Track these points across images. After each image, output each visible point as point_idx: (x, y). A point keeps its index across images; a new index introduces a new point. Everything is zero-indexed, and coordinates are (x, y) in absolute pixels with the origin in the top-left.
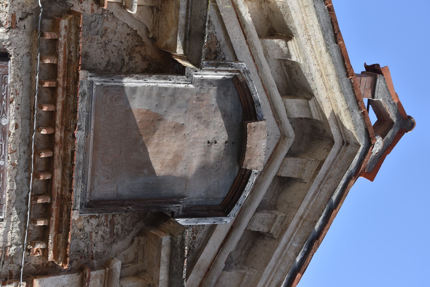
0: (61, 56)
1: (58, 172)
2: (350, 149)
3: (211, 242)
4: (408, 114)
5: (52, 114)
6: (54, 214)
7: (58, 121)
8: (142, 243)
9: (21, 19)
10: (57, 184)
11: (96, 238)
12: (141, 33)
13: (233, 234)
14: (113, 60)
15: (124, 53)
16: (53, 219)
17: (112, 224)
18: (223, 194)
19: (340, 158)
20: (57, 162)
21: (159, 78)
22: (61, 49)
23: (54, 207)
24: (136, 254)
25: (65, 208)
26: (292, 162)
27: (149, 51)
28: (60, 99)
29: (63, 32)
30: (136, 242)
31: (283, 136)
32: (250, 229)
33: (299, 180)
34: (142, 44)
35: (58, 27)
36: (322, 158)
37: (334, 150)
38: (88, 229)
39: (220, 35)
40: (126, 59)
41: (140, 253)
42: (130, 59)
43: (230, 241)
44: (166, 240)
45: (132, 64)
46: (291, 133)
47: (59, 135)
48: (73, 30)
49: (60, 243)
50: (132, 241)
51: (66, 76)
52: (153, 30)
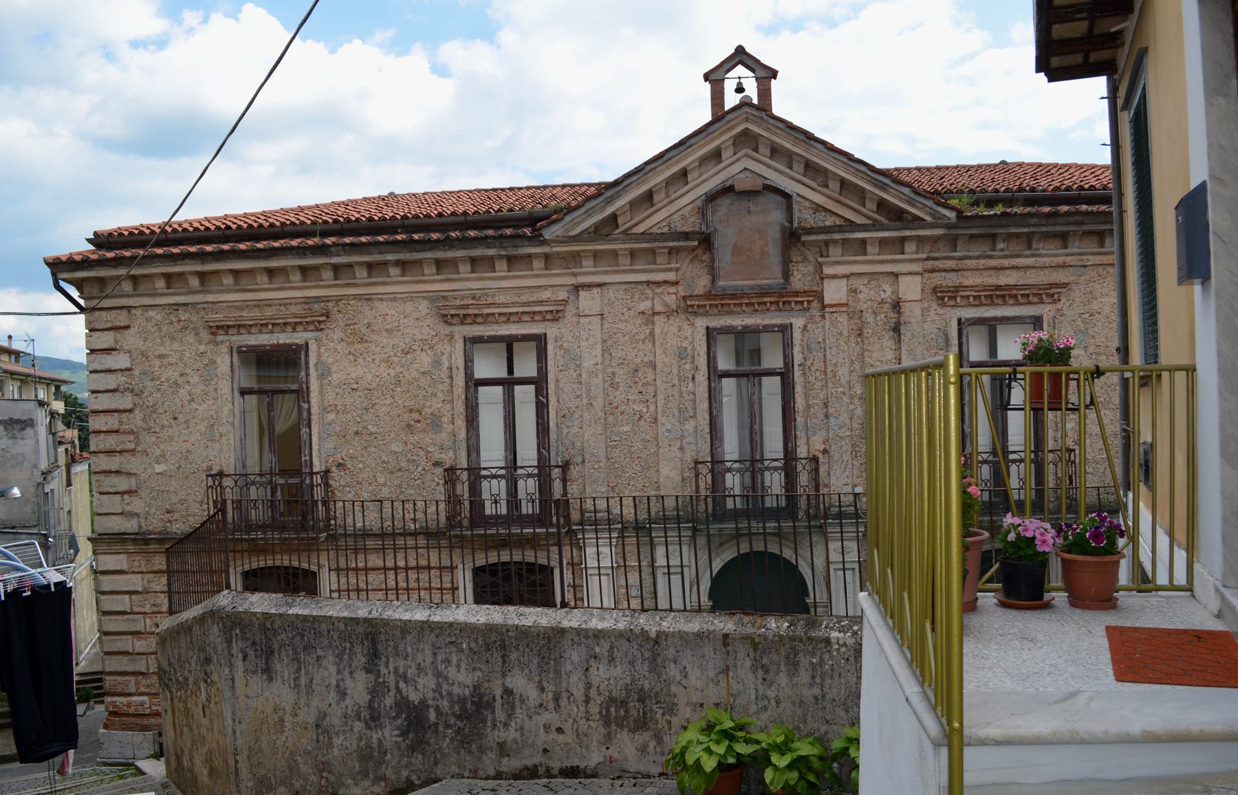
1: (765, 299)
2: (751, 117)
3: (779, 429)
10: (772, 299)
11: (805, 271)
12: (691, 257)
16: (791, 299)
18: (779, 198)
20: (760, 300)
26: (761, 149)
27: (699, 251)
29: (693, 303)
31: (746, 155)
32: (791, 261)
34: (697, 255)
38: (800, 276)
39: (689, 208)
46: (744, 151)
51: (715, 300)
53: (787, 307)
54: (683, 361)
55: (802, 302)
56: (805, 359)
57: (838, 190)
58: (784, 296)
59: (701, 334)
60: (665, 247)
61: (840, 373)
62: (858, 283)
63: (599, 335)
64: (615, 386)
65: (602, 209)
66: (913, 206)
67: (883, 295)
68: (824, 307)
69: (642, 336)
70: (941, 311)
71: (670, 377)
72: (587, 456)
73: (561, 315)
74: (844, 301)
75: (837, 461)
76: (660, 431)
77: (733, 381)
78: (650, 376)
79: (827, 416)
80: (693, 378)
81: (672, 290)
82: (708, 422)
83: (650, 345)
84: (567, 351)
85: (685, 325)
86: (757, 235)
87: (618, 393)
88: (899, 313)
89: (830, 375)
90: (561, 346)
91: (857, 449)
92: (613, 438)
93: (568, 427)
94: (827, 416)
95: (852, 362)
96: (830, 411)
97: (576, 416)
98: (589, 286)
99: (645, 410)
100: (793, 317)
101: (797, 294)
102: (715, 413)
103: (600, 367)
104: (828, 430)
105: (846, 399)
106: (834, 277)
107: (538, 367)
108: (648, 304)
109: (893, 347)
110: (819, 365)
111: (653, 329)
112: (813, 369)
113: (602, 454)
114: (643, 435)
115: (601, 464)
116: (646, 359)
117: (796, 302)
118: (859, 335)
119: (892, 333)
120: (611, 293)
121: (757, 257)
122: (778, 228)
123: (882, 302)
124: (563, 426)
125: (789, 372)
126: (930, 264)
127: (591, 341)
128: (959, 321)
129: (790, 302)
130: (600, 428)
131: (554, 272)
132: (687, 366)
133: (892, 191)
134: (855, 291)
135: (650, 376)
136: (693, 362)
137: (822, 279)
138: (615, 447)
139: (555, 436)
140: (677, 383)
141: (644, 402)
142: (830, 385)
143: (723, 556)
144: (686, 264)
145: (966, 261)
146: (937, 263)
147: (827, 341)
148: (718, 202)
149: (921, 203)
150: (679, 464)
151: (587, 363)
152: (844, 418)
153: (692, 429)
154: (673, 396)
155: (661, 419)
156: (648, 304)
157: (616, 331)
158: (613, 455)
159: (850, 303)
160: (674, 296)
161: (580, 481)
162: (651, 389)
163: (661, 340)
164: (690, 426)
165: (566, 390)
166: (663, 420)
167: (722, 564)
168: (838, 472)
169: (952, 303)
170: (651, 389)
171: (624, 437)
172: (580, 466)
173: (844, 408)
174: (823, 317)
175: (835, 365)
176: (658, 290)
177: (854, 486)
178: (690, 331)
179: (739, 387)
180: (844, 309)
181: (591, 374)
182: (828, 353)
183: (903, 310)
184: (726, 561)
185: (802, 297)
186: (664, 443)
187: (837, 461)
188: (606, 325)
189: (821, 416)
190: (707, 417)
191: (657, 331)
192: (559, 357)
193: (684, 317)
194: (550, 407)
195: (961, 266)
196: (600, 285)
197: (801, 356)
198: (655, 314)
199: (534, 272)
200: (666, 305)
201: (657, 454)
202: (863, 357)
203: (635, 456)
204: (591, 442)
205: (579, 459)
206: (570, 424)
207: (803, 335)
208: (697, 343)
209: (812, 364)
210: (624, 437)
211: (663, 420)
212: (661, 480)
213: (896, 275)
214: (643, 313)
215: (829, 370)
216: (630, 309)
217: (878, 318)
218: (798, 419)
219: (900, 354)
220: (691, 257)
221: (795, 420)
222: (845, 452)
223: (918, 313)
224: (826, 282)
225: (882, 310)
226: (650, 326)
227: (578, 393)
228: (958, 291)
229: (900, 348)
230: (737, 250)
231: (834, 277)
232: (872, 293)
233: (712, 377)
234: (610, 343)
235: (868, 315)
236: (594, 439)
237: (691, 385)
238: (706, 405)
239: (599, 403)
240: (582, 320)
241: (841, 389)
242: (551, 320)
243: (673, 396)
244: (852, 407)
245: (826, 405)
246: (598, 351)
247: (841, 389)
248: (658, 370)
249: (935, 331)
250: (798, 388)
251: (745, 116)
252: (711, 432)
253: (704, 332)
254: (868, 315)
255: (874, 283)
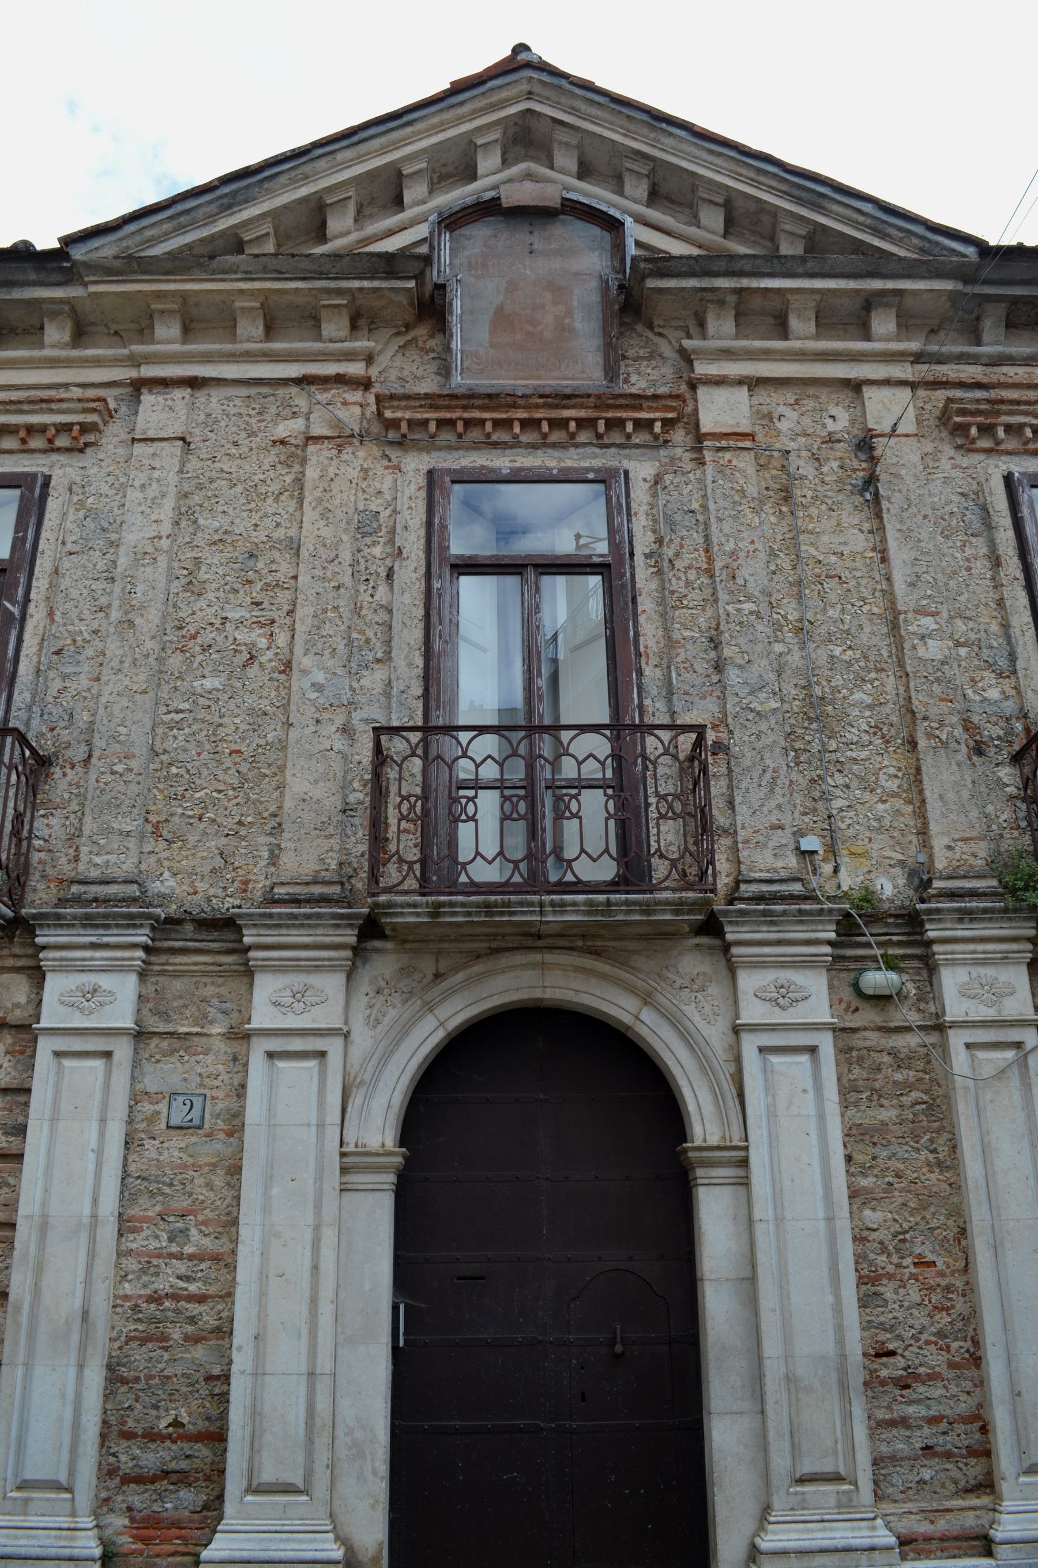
0: (426, 416)
1: (566, 413)
2: (537, 89)
4: (509, 53)
5: (497, 423)
6: (619, 415)
7: (504, 416)
8: (662, 323)
9: (390, 460)
10: (582, 414)
13: (653, 222)
14: (435, 369)
15: (426, 358)
17: (638, 358)
18: (596, 231)
19: (548, 99)
20: (554, 414)
21: (451, 313)
22: (419, 416)
23: (610, 415)
24: (676, 328)
25: (611, 401)
28: (477, 414)
29: (399, 414)
30: (661, 330)
33: (579, 147)
34: (415, 339)
35: (393, 420)
36: (550, 122)
37: (538, 107)
40: (432, 355)
41: (675, 323)
42: (433, 351)
43: (661, 225)
44: (651, 283)
45: (440, 349)
47: (522, 414)
48: (395, 403)
49: (655, 405)
50: (660, 335)
52: (396, 327)
53: (616, 437)
54: (368, 540)
55: (650, 423)
56: (660, 541)
57: (722, 232)
58: (609, 407)
59: (413, 487)
60: (339, 292)
61: (744, 573)
62: (776, 401)
63: (173, 478)
64: (193, 587)
65: (211, 218)
66: (885, 236)
67: (831, 426)
68: (700, 438)
69: (275, 488)
70: (965, 461)
71: (331, 567)
72: (99, 743)
73: (91, 438)
74: (747, 429)
75: (749, 769)
76: (295, 688)
77: (489, 582)
78: (285, 569)
79: (719, 667)
80: (390, 575)
81: (357, 396)
82: (420, 671)
83: (292, 505)
84: (91, 513)
85: (379, 468)
86: (548, 295)
87: (202, 603)
88: (873, 460)
89: (720, 575)
90: (81, 504)
91: (798, 745)
92: (174, 705)
93: (65, 677)
94: (719, 667)
95: (773, 554)
96: (727, 652)
97: (90, 652)
98: (165, 383)
99: (263, 642)
100: (629, 457)
101: (637, 401)
102: (437, 645)
103: (165, 543)
104: (723, 698)
105: (762, 628)
106: (720, 382)
107: (15, 540)
108: (297, 425)
109: (866, 526)
110: (692, 556)
111: (303, 473)
112: (679, 564)
113: (139, 739)
114: (250, 700)
115: (134, 764)
116: (279, 534)
117: (638, 424)
118: (786, 499)
119: (858, 500)
120: (213, 400)
121: (548, 335)
122: (594, 284)
123: (831, 440)
124: (52, 674)
125: (622, 564)
126: (923, 370)
127: (153, 491)
128: (1008, 480)
129: (621, 423)
130: (142, 677)
131: (90, 352)
132: (377, 551)
133: (835, 207)
134: (769, 416)
135: (285, 569)
136: (391, 542)
137: (693, 386)
138: (178, 725)
139: (27, 696)
140: (347, 579)
141: (262, 625)
142: (723, 596)
143: (444, 1011)
144: (389, 354)
145: (1005, 369)
146: (943, 369)
147: (712, 506)
148: (466, 231)
149: (900, 229)
150: (337, 767)
151: (133, 536)
152: (762, 668)
153: (379, 688)
154: (336, 608)
155: (303, 661)
156: (297, 425)
157: (214, 474)
158: (170, 744)
159: (760, 437)
160: (357, 410)
161: (74, 806)
162: (283, 597)
163: (318, 493)
164: (374, 679)
165: (74, 593)
166: (307, 662)
167: (441, 1034)
168: (755, 797)
169: (985, 443)
170: (283, 597)
171: (202, 701)
172: (79, 769)
173: (759, 648)
174: (701, 462)
175: (733, 554)
176: (323, 397)
177: (800, 833)
178: (389, 480)
179: (501, 594)
180: (748, 444)
181: (139, 557)
182: (714, 528)
183: (878, 453)
184: (453, 1024)
185: (650, 409)
186: (302, 714)
187: (749, 769)
188: (193, 464)
189: (701, 667)
190: (420, 662)
191: (312, 473)
192: (69, 526)
193: (376, 451)
194: (30, 625)
195: (994, 379)
196: (194, 383)
197: (651, 537)
198: (310, 439)
199: (47, 352)
200: (338, 424)
201: (282, 746)
202: (797, 546)
203: (225, 748)
204: (116, 710)
205: (78, 752)
206: (69, 669)
207: (655, 495)
208: (402, 503)
209: (677, 555)
210: (202, 701)
211: (307, 662)
212: (288, 804)
213: (855, 386)
214: (283, 442)
215: (718, 564)
216: (252, 434)
217: (825, 469)
218: (647, 671)
219: (884, 540)
220: (401, 341)
221: (640, 673)
222: (771, 748)
223: (915, 458)
224: (702, 392)
225: (832, 454)
226: (297, 468)
227: (103, 601)
228: (998, 413)
229: (882, 528)
230: (502, 319)
231: (720, 382)
232: (807, 421)
233: (435, 567)
234: (197, 499)
235: (802, 463)
236: (124, 703)
237: (382, 590)
238: (417, 634)
239: (149, 621)
240: (139, 449)
241: (748, 606)
242: (68, 450)
243: (336, 608)
244: (778, 648)
245: (715, 643)
246: (166, 511)
247: (748, 606)
248: (304, 553)
249: (956, 499)
250: (646, 604)
251: (525, 87)
252: (426, 696)
253: (422, 481)
254: (802, 463)
255: (809, 404)
